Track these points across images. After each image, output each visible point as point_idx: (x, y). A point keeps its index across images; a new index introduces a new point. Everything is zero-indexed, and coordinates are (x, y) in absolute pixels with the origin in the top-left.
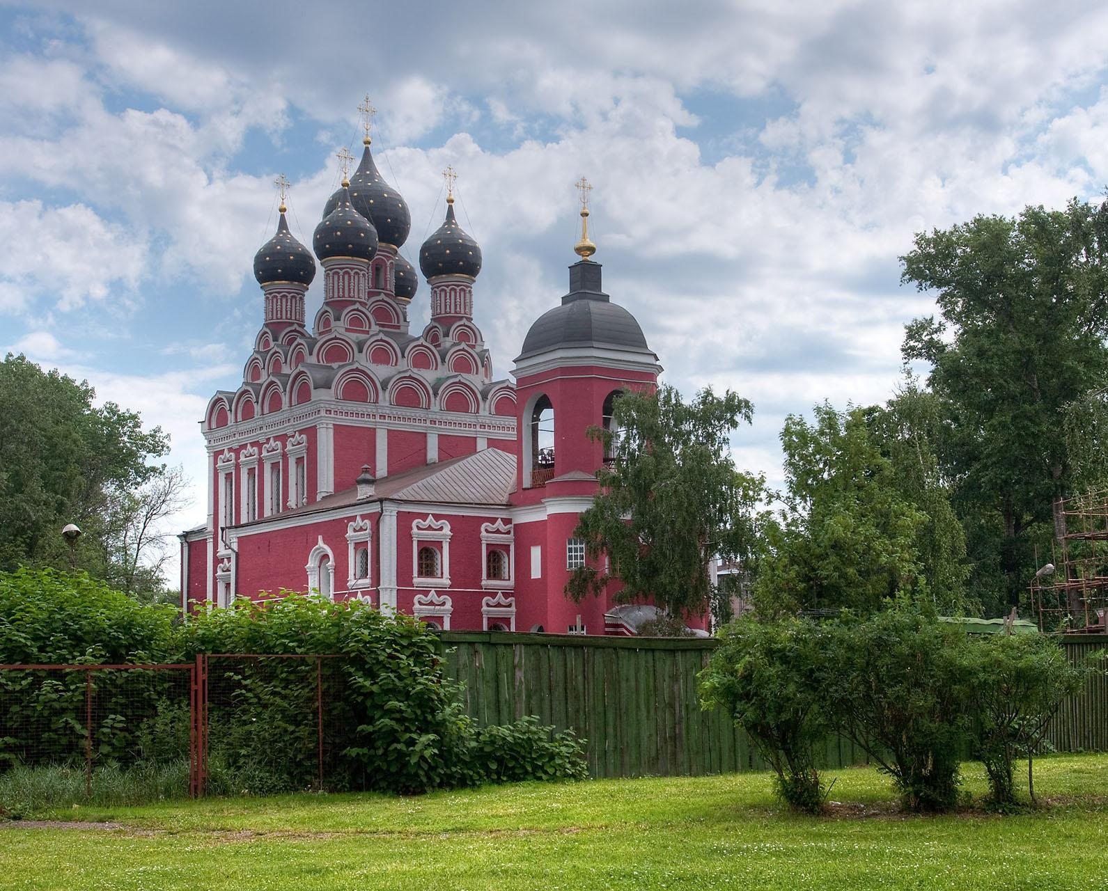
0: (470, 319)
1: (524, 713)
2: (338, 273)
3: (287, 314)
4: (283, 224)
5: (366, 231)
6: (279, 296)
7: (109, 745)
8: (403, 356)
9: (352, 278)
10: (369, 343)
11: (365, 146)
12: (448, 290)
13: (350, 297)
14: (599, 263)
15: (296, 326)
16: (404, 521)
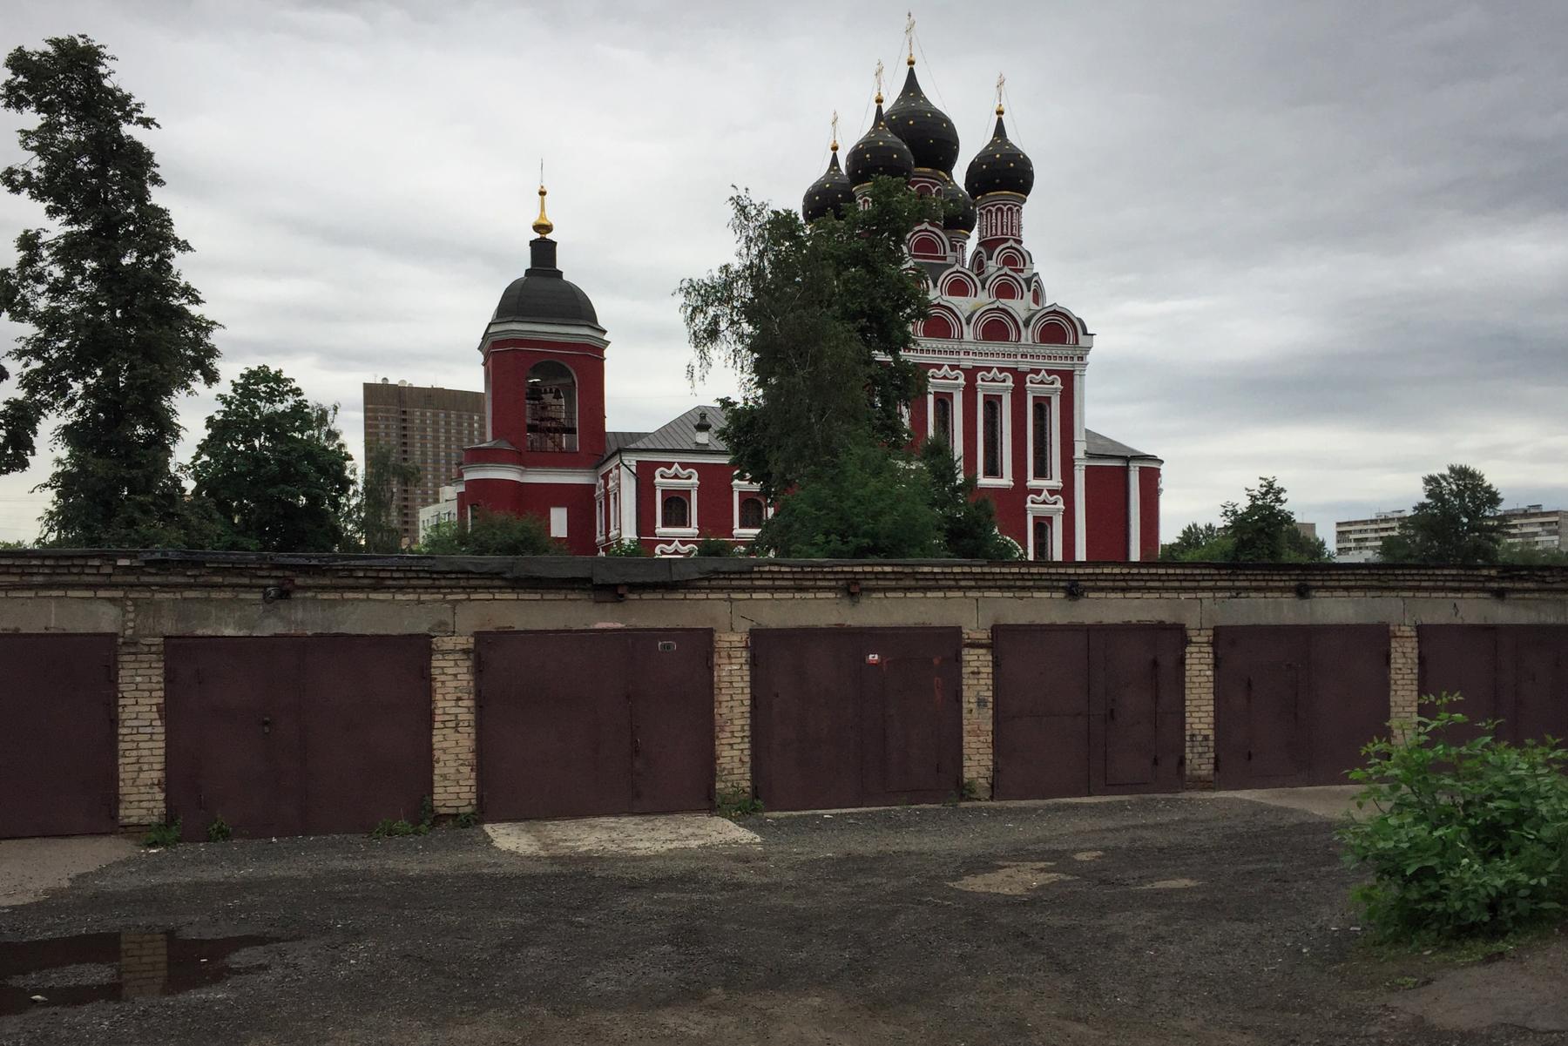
0: (1020, 242)
4: (1000, 130)
5: (899, 151)
15: (1011, 243)
16: (644, 476)
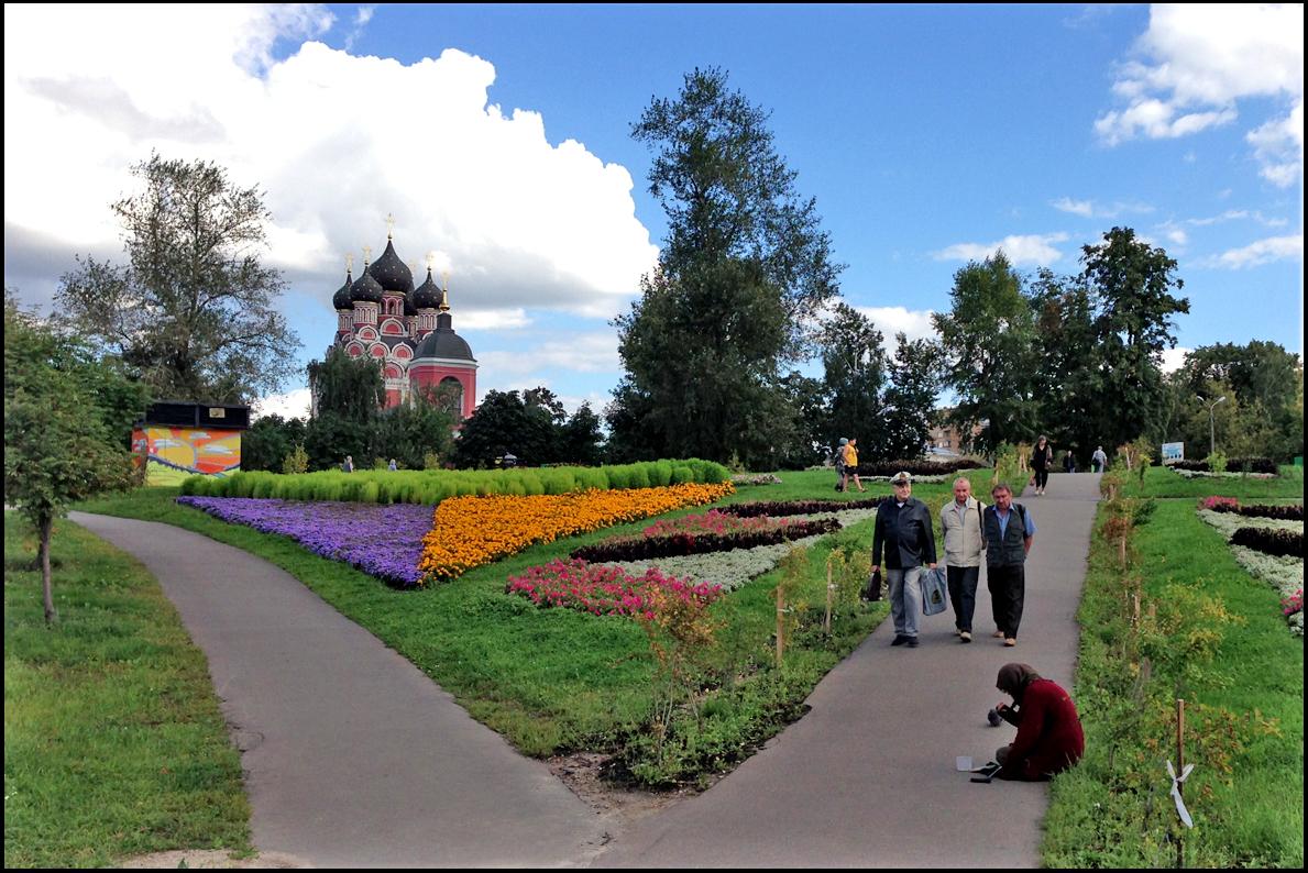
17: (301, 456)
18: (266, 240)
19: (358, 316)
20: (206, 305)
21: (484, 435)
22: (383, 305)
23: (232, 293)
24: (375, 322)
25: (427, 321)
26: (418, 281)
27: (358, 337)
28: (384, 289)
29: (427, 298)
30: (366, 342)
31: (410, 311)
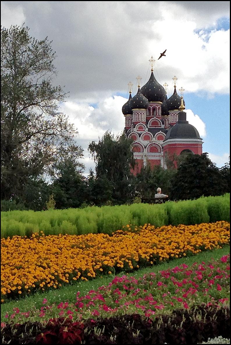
1: (10, 38)
2: (135, 114)
3: (139, 119)
6: (128, 119)
7: (92, 174)
8: (154, 137)
9: (139, 115)
10: (143, 134)
11: (130, 94)
12: (139, 113)
13: (142, 120)
14: (186, 112)
17: (51, 202)
18: (54, 70)
19: (134, 118)
20: (22, 112)
21: (186, 182)
22: (149, 110)
23: (37, 104)
24: (144, 120)
25: (173, 117)
26: (169, 93)
27: (135, 130)
28: (149, 101)
29: (174, 104)
30: (139, 132)
31: (165, 112)
